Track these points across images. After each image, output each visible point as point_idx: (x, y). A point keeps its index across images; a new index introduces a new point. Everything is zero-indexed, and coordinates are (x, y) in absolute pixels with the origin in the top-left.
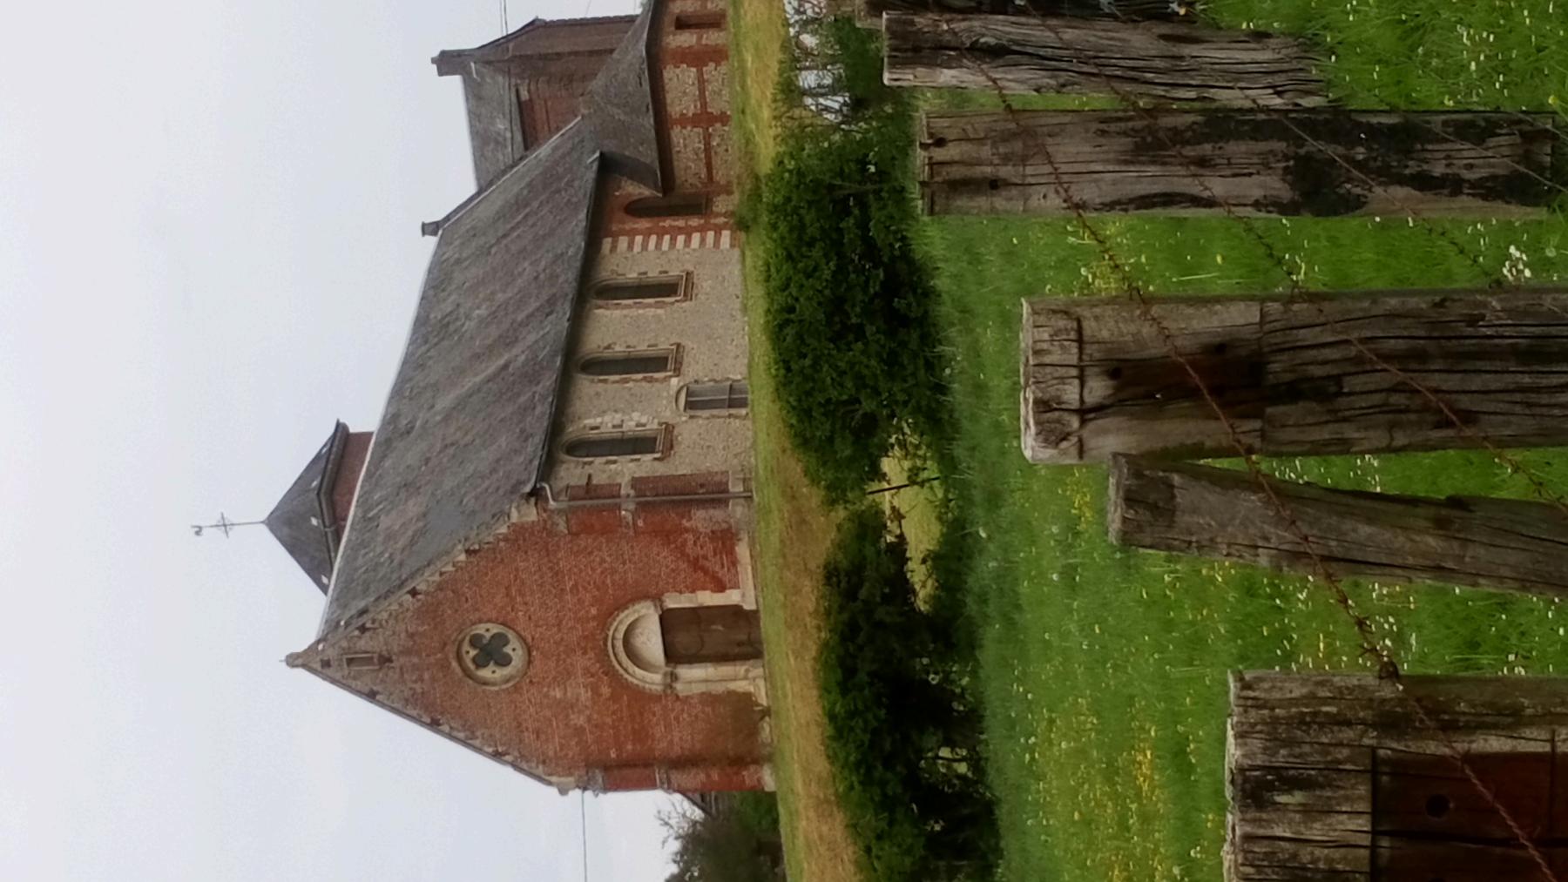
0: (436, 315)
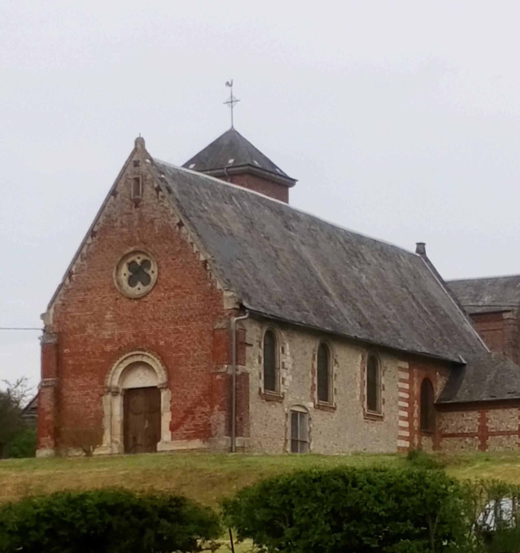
0: (364, 249)
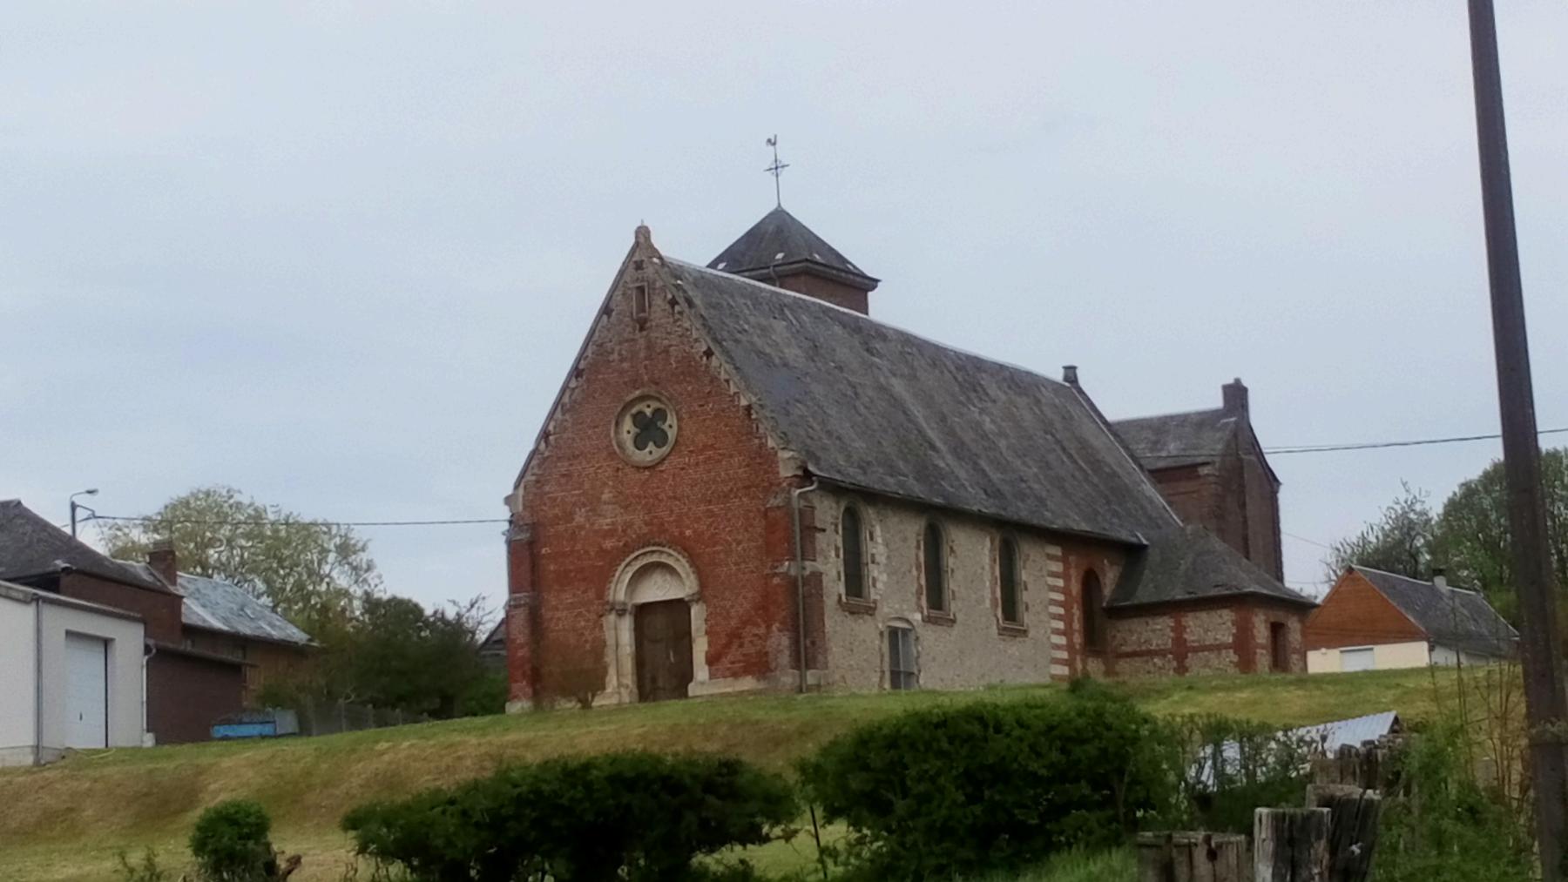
0: (985, 380)
